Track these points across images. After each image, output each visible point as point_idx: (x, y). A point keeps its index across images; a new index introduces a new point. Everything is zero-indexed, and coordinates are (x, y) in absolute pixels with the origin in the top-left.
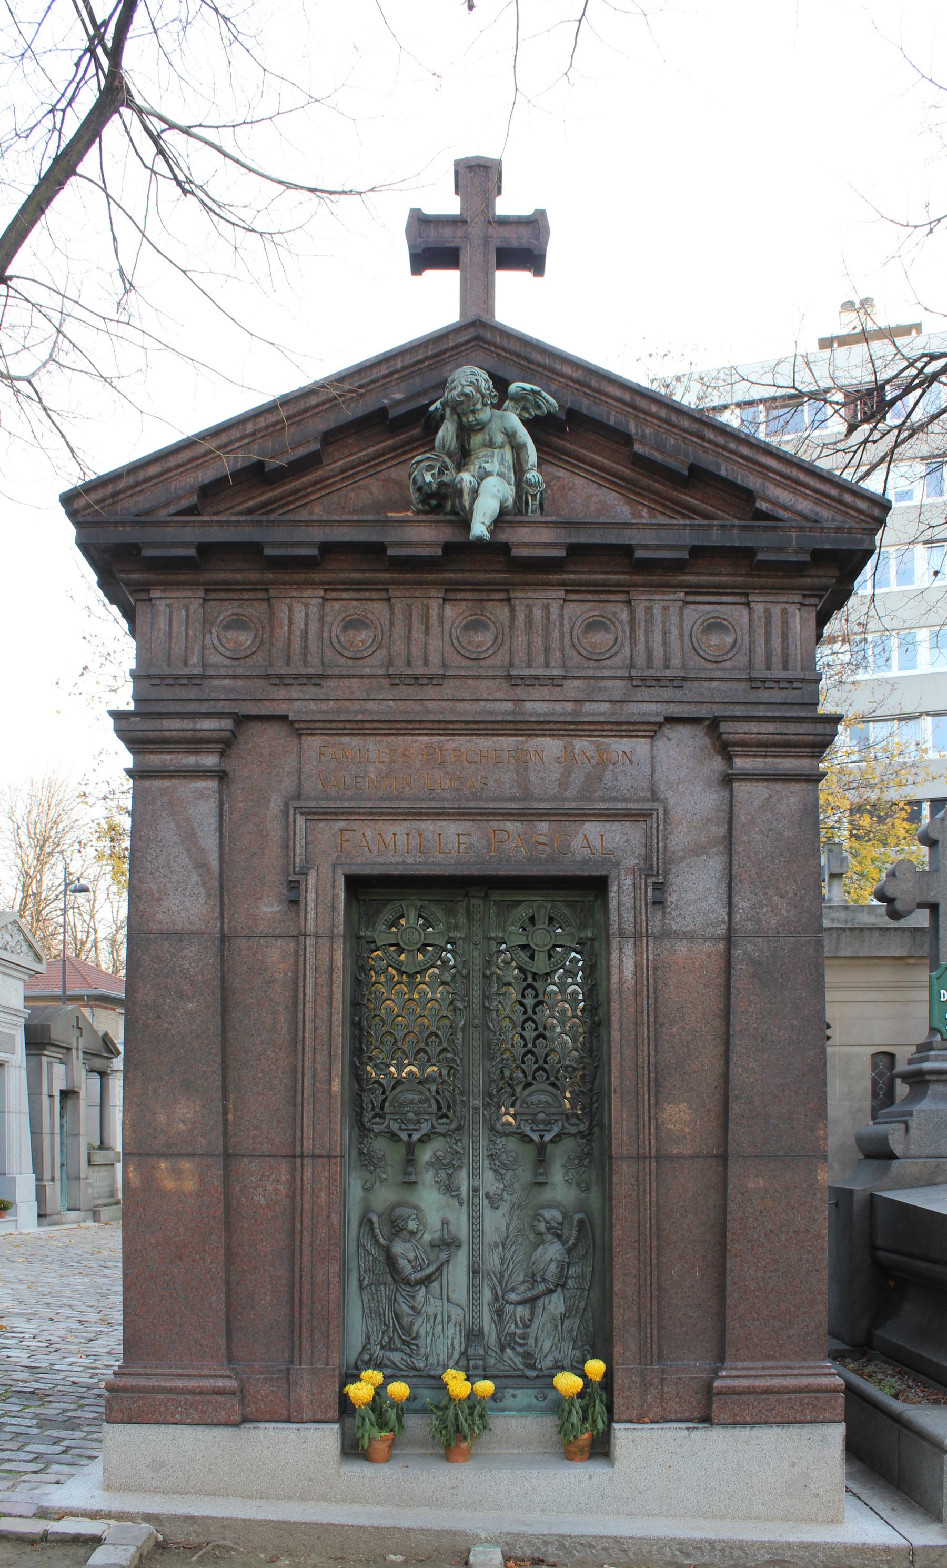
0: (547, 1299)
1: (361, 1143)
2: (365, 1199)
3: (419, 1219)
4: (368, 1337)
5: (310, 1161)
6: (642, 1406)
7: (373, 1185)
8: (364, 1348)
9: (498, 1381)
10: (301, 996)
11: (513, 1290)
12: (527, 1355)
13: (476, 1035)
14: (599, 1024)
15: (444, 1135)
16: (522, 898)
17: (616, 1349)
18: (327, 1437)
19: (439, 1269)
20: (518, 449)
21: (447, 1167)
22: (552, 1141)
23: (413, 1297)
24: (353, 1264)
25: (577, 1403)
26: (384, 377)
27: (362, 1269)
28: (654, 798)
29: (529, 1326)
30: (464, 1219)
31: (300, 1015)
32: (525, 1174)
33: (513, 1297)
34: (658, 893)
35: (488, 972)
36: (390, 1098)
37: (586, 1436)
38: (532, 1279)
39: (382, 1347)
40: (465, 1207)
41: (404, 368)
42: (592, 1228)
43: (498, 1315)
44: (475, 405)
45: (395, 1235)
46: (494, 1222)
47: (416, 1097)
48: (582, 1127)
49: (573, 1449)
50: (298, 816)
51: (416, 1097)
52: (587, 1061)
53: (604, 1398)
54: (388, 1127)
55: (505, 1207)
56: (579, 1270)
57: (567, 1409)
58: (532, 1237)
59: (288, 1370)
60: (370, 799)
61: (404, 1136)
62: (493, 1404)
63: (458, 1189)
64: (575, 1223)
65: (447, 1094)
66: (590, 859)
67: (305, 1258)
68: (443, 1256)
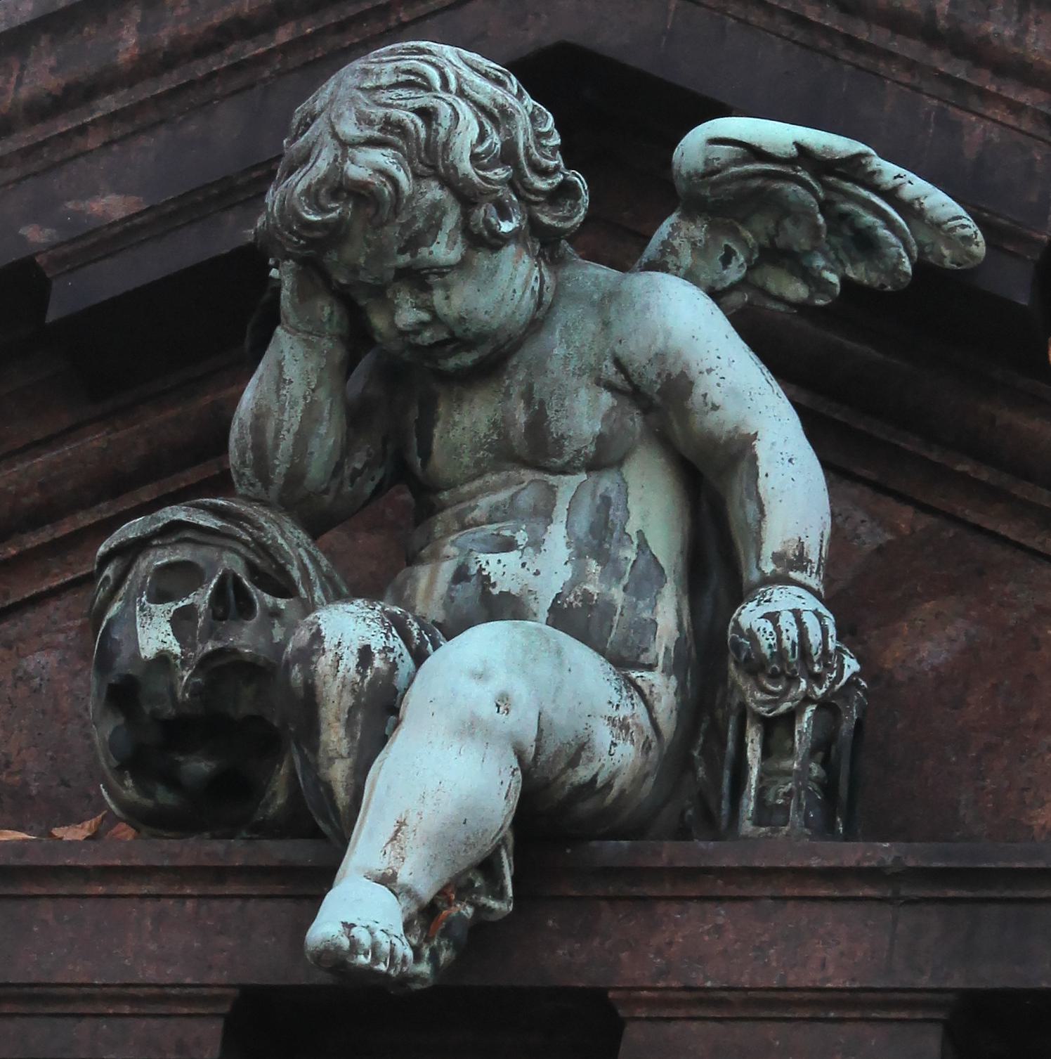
20: (711, 478)
26: (42, 110)
41: (152, 63)
44: (414, 242)
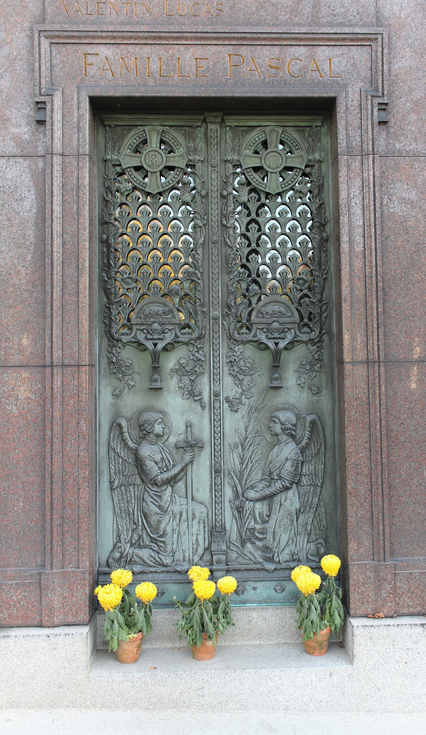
0: (283, 496)
1: (110, 353)
2: (114, 405)
3: (165, 423)
4: (119, 536)
5: (60, 370)
6: (377, 601)
7: (121, 392)
8: (115, 546)
9: (239, 575)
10: (48, 211)
11: (252, 487)
12: (266, 549)
13: (215, 251)
14: (327, 240)
15: (186, 344)
16: (256, 124)
17: (350, 545)
18: (79, 639)
19: (184, 469)
21: (189, 373)
22: (286, 348)
23: (160, 497)
24: (104, 467)
25: (316, 598)
27: (112, 471)
28: (379, 23)
29: (267, 522)
30: (206, 421)
31: (48, 230)
32: (261, 379)
33: (252, 494)
34: (383, 113)
35: (225, 193)
36: (136, 310)
37: (325, 631)
38: (270, 477)
39: (132, 545)
40: (207, 410)
42: (323, 428)
43: (239, 512)
45: (143, 438)
46: (234, 424)
47: (161, 309)
48: (313, 335)
49: (313, 644)
50: (43, 39)
51: (161, 309)
52: (316, 273)
53: (340, 593)
54: (135, 337)
55: (243, 410)
56: (312, 468)
57: (307, 606)
58: (269, 437)
59: (40, 574)
60: (112, 23)
61: (149, 345)
62: (236, 596)
63: (200, 394)
64: (308, 424)
65: (189, 305)
66: (319, 82)
67: (56, 464)
68: (187, 457)
